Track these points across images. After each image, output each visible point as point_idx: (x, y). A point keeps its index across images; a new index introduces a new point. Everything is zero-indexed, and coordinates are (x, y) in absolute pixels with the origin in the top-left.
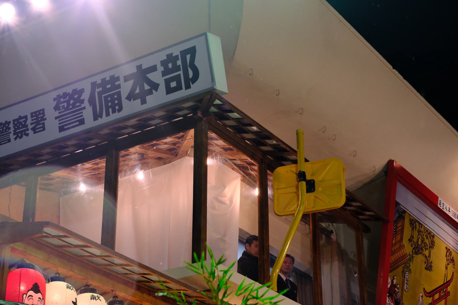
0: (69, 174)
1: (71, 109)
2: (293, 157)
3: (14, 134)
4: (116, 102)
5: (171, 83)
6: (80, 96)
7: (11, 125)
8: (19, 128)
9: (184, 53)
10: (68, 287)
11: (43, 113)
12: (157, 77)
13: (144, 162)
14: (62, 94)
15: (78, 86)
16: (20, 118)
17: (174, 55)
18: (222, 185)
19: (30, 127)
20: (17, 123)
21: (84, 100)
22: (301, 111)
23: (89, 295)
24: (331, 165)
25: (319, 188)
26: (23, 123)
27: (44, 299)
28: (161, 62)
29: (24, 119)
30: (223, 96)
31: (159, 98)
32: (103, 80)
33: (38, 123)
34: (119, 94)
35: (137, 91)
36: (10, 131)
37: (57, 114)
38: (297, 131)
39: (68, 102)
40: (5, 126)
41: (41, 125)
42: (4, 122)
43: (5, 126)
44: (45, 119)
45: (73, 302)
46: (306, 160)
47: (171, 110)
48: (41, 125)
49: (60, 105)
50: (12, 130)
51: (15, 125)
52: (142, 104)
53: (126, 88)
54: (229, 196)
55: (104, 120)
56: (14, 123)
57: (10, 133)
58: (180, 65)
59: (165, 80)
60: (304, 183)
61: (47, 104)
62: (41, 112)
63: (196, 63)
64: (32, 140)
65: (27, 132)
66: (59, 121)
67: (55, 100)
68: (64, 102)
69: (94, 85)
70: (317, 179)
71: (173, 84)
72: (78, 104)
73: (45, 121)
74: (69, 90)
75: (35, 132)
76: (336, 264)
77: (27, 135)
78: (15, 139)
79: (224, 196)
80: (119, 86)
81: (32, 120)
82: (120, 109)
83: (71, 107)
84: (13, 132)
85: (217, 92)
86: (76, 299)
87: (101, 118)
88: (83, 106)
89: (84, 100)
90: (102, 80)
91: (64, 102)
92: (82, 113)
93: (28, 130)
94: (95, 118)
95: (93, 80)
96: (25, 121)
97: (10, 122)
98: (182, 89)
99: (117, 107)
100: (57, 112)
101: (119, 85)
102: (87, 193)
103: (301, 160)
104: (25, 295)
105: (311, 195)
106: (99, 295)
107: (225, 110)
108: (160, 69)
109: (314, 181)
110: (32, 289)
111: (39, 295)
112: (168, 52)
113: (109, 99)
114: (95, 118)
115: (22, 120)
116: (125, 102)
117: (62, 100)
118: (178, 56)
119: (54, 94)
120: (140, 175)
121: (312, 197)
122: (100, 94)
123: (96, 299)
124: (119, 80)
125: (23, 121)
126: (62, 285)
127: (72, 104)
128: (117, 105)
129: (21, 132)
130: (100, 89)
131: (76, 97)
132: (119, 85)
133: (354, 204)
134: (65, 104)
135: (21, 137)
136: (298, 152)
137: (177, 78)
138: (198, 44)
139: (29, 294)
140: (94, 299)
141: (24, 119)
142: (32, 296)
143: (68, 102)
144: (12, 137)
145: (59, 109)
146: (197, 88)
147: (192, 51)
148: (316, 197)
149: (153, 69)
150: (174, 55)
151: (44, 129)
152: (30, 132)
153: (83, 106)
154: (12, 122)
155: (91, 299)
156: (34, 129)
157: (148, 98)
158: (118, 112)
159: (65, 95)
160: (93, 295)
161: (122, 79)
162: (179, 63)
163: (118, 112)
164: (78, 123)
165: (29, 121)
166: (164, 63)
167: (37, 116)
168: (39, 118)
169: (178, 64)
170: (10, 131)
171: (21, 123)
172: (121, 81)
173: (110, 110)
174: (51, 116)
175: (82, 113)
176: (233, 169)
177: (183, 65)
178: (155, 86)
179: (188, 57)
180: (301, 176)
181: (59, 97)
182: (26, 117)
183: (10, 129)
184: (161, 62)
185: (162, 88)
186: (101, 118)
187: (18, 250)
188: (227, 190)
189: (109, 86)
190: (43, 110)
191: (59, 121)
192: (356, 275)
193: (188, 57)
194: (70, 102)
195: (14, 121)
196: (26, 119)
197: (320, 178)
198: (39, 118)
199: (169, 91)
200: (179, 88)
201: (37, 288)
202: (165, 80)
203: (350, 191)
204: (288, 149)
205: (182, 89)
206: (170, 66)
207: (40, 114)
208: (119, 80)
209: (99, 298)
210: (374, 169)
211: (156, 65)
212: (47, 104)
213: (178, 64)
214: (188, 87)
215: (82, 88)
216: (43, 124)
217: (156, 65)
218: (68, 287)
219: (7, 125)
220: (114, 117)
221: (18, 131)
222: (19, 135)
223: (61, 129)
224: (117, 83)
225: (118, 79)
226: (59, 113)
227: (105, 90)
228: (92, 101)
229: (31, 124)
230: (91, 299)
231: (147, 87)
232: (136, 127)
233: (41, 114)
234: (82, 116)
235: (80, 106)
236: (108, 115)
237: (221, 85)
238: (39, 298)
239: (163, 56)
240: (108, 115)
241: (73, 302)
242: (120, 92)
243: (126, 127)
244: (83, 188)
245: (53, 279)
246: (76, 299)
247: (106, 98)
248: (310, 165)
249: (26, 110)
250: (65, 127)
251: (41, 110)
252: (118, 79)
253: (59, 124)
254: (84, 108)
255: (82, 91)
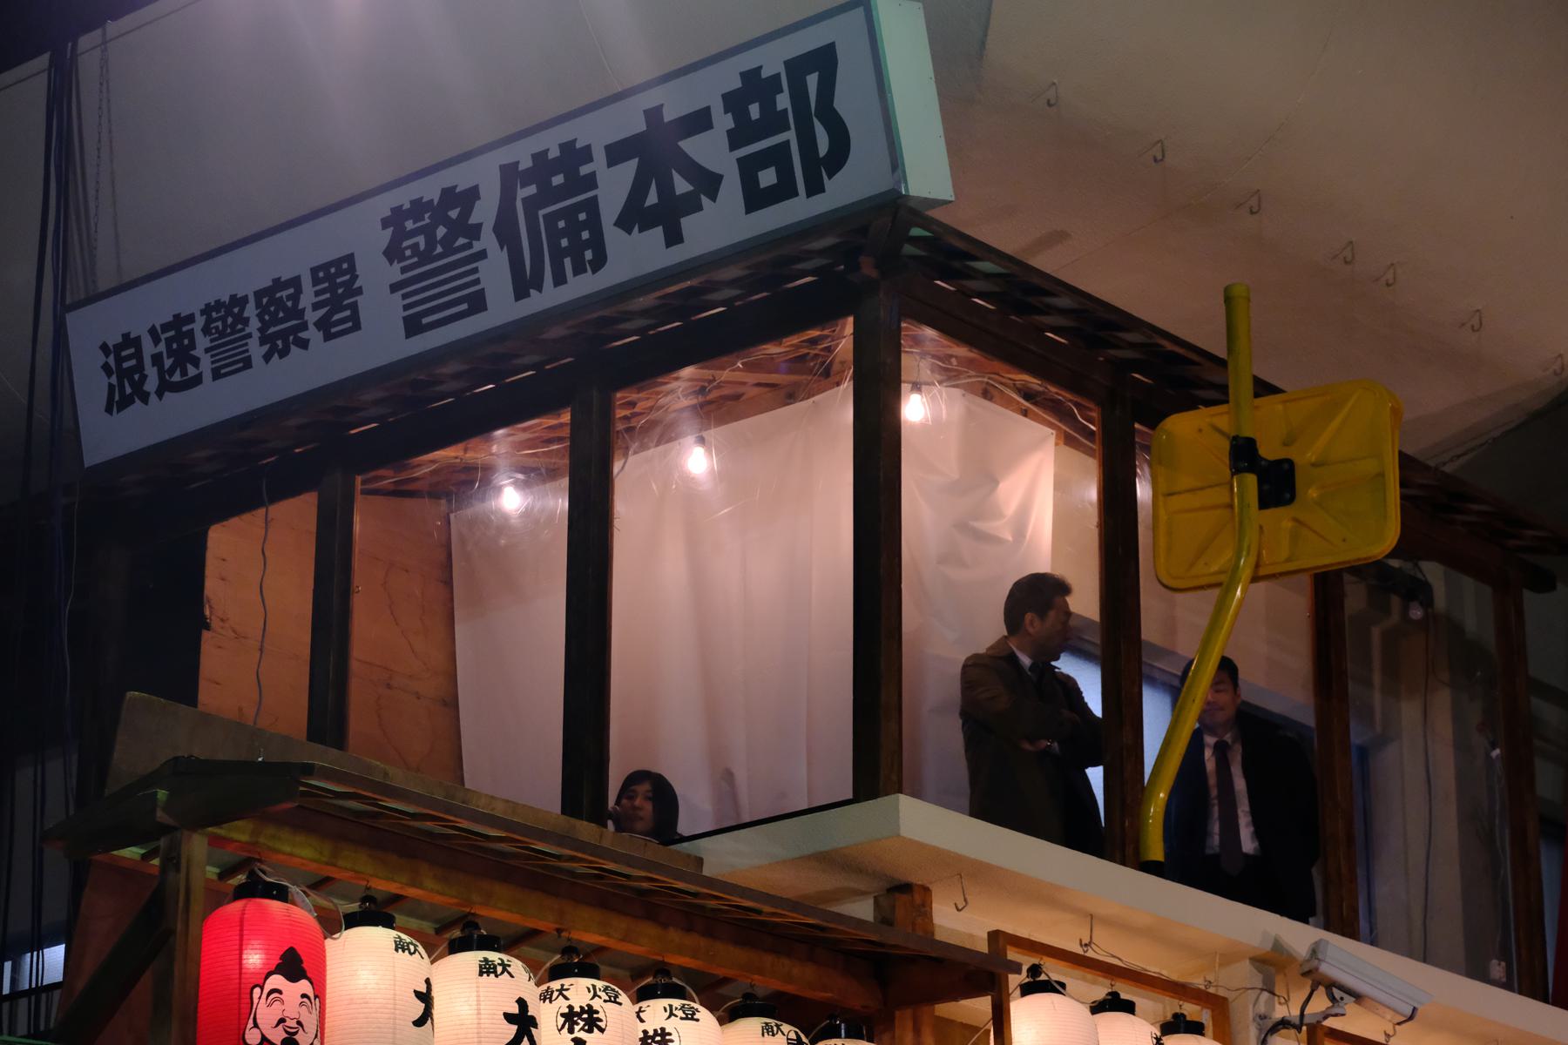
0: (466, 450)
1: (441, 256)
2: (1216, 378)
3: (262, 342)
4: (585, 235)
5: (760, 174)
6: (467, 211)
7: (251, 311)
8: (276, 321)
9: (798, 68)
10: (400, 946)
11: (352, 268)
12: (711, 150)
13: (717, 409)
14: (407, 206)
15: (460, 177)
16: (278, 284)
17: (765, 74)
18: (982, 473)
19: (312, 317)
20: (269, 303)
21: (479, 226)
22: (1253, 202)
23: (472, 959)
24: (1349, 404)
25: (1309, 492)
26: (289, 304)
27: (320, 994)
28: (725, 97)
29: (291, 291)
30: (935, 213)
31: (720, 225)
32: (540, 157)
33: (335, 304)
34: (592, 206)
35: (652, 198)
36: (248, 330)
37: (394, 273)
38: (1227, 290)
39: (428, 232)
40: (229, 313)
41: (348, 313)
42: (226, 299)
43: (229, 313)
44: (359, 291)
45: (418, 994)
46: (1263, 388)
47: (769, 260)
48: (348, 313)
49: (405, 244)
50: (254, 324)
51: (262, 311)
52: (669, 244)
53: (613, 186)
54: (1011, 507)
55: (548, 297)
56: (258, 305)
57: (249, 336)
58: (786, 110)
59: (738, 160)
60: (1251, 480)
61: (362, 235)
62: (345, 266)
63: (841, 104)
64: (321, 364)
65: (303, 335)
66: (405, 297)
67: (385, 223)
68: (414, 233)
69: (510, 175)
70: (1303, 457)
71: (768, 177)
72: (461, 241)
73: (358, 298)
74: (430, 190)
75: (328, 337)
76: (1443, 699)
77: (304, 344)
78: (267, 358)
79: (997, 514)
80: (591, 182)
81: (317, 294)
82: (599, 262)
83: (439, 249)
84: (256, 335)
85: (912, 204)
86: (428, 981)
87: (540, 289)
88: (477, 246)
89: (479, 226)
90: (535, 157)
91: (414, 233)
92: (476, 270)
93: (304, 327)
94: (521, 293)
95: (505, 156)
96: (295, 298)
97: (245, 300)
98: (797, 194)
99: (589, 255)
100: (397, 266)
101: (593, 175)
102: (526, 514)
103: (1241, 387)
104: (257, 991)
105: (1281, 518)
106: (505, 957)
107: (950, 254)
108: (723, 121)
109: (1290, 462)
110: (278, 970)
111: (304, 986)
112: (747, 61)
113: (561, 224)
114: (521, 293)
115: (284, 294)
116: (613, 237)
117: (409, 225)
118: (777, 77)
119: (383, 205)
120: (697, 461)
121: (1287, 524)
122: (532, 205)
123: (495, 972)
124: (591, 160)
125: (289, 297)
126: (378, 938)
127: (444, 241)
128: (587, 244)
129: (283, 335)
130: (532, 190)
131: (454, 214)
132: (593, 175)
133: (1476, 507)
134: (421, 240)
135: (284, 353)
136: (1230, 367)
137: (779, 156)
138: (843, 33)
139: (267, 988)
140: (488, 973)
141: (291, 291)
142: (280, 992)
143: (428, 232)
144: (256, 350)
145: (402, 258)
146: (843, 190)
147: (825, 60)
148: (1296, 520)
149: (699, 121)
150: (765, 74)
151: (357, 326)
152: (313, 334)
153: (477, 246)
154: (252, 299)
155: (481, 974)
156: (324, 325)
157: (688, 223)
158: (594, 272)
159: (419, 207)
160: (486, 960)
161: (600, 156)
162: (783, 101)
163: (594, 272)
164: (464, 306)
165: (307, 298)
166: (734, 102)
167: (330, 278)
168: (339, 280)
169: (780, 107)
170: (248, 330)
171: (279, 303)
172: (599, 163)
173: (568, 262)
174: (377, 276)
175: (476, 270)
176: (1025, 413)
177: (795, 111)
178: (709, 183)
179: (812, 81)
180: (1243, 454)
181: (395, 219)
182: (295, 282)
183: (246, 321)
184: (725, 97)
185: (732, 188)
186: (540, 289)
187: (232, 841)
188: (1004, 487)
189: (558, 180)
190: (350, 258)
191: (405, 297)
192: (1498, 751)
193: (812, 81)
194: (433, 232)
195: (259, 295)
196: (299, 291)
197: (1311, 456)
198: (339, 280)
199: (756, 199)
200: (783, 191)
201: (292, 965)
202: (738, 160)
203: (1448, 469)
204: (1195, 357)
205: (797, 194)
206: (754, 111)
207: (341, 273)
208: (591, 160)
209: (505, 967)
210: (1556, 367)
211: (708, 109)
212: (362, 235)
213: (780, 107)
214: (815, 188)
215: (471, 184)
216: (354, 307)
217: (708, 109)
218: (400, 946)
219: (236, 310)
220: (581, 286)
221: (272, 330)
222: (281, 343)
223: (413, 327)
224: (585, 170)
225: (586, 155)
226: (404, 270)
227: (547, 195)
228: (505, 231)
229: (316, 306)
230: (481, 974)
231: (682, 186)
232: (666, 310)
233: (344, 273)
234: (477, 281)
235: (469, 246)
236: (560, 280)
237: (928, 174)
238: (304, 996)
239: (728, 77)
240: (560, 280)
241: (418, 994)
242: (595, 198)
243: (629, 316)
244: (510, 499)
245: (353, 921)
246: (428, 981)
247: (551, 219)
248: (1280, 407)
249: (294, 256)
250: (425, 321)
251: (337, 263)
252: (586, 155)
253: (406, 308)
254: (482, 255)
255: (473, 194)
